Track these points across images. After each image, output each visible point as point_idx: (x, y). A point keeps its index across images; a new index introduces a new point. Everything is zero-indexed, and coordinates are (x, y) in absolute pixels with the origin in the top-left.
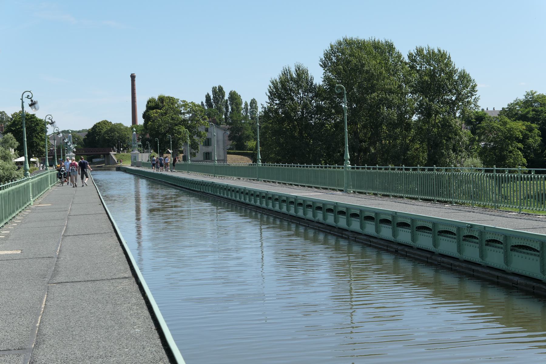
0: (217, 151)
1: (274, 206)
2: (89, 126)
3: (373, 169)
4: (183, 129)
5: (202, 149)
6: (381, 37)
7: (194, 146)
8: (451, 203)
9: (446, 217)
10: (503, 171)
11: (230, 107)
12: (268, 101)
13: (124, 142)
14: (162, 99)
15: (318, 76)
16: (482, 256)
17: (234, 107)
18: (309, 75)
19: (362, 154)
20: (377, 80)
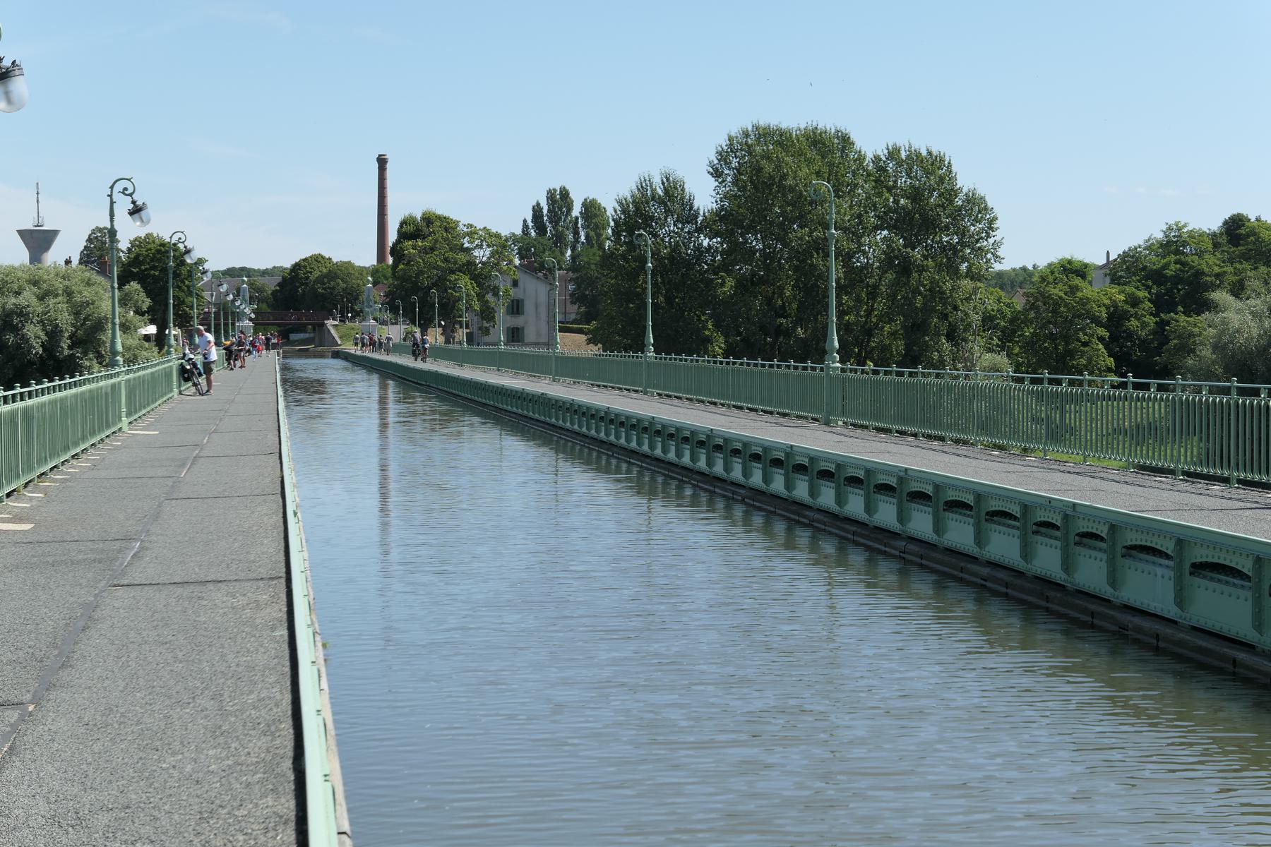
0: (534, 325)
1: (694, 459)
2: (287, 261)
3: (911, 374)
5: (503, 319)
6: (828, 121)
7: (487, 314)
9: (1252, 534)
11: (582, 234)
14: (429, 219)
15: (705, 196)
16: (1113, 581)
17: (592, 233)
19: (781, 339)
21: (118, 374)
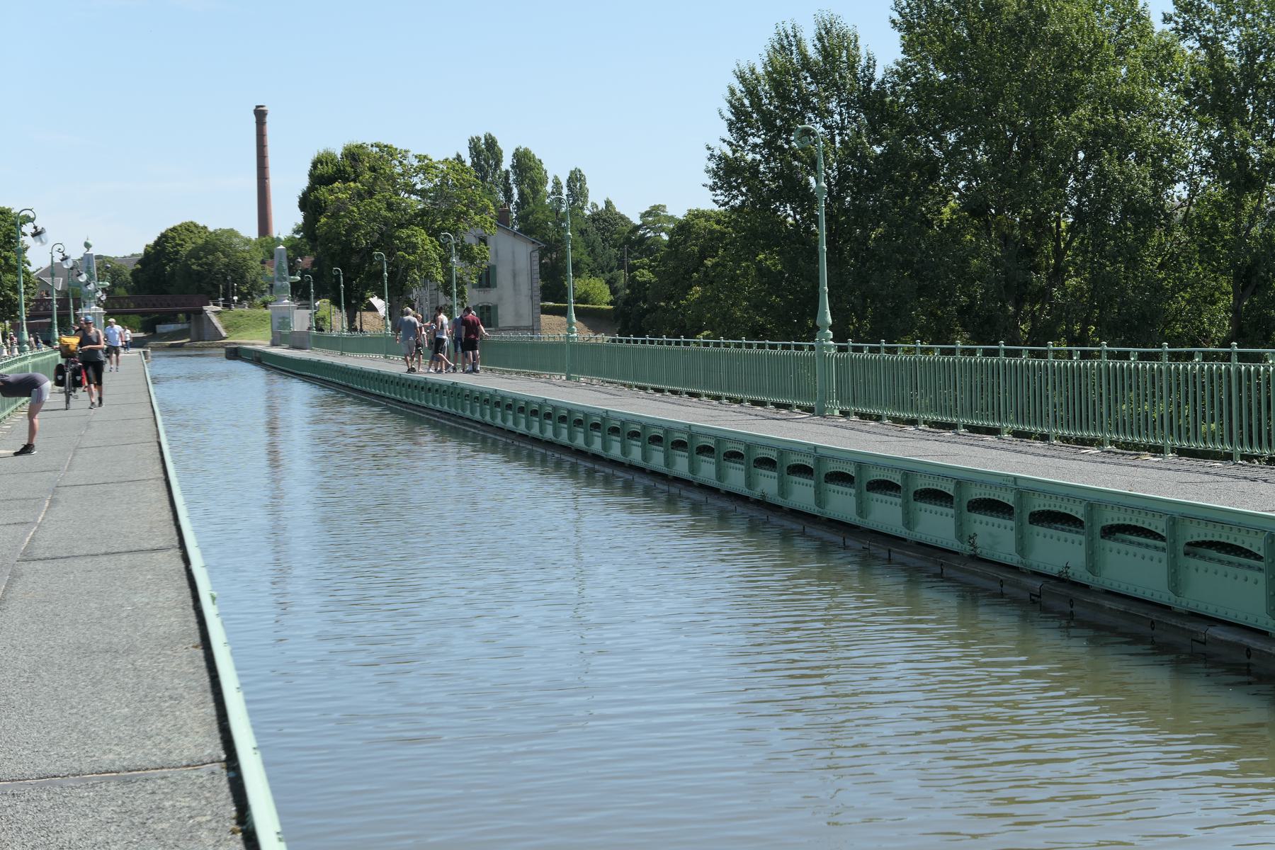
4: (421, 237)
8: (1044, 438)
10: (1126, 356)
11: (515, 191)
12: (728, 136)
13: (242, 279)
14: (353, 154)
17: (527, 191)
18: (862, 52)
20: (1088, 70)
21: (26, 358)
